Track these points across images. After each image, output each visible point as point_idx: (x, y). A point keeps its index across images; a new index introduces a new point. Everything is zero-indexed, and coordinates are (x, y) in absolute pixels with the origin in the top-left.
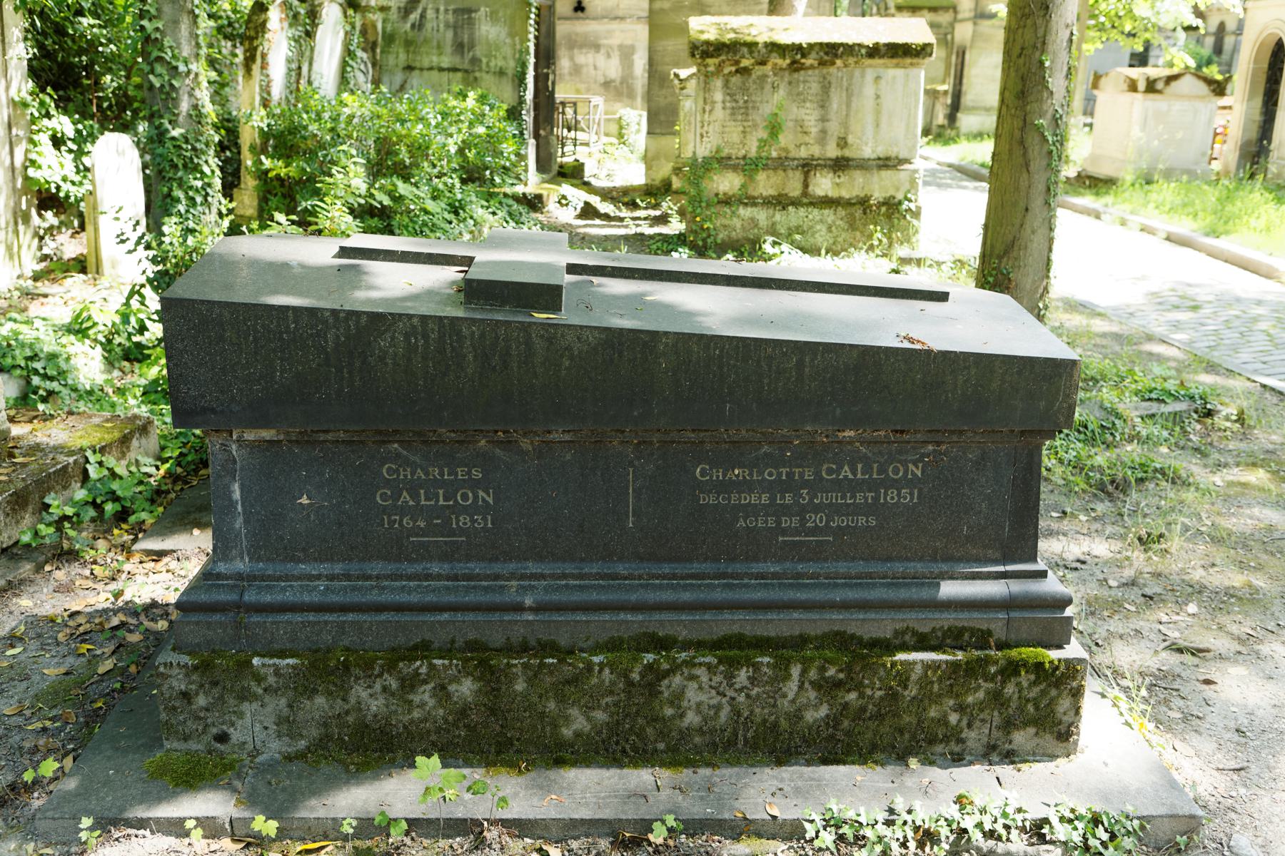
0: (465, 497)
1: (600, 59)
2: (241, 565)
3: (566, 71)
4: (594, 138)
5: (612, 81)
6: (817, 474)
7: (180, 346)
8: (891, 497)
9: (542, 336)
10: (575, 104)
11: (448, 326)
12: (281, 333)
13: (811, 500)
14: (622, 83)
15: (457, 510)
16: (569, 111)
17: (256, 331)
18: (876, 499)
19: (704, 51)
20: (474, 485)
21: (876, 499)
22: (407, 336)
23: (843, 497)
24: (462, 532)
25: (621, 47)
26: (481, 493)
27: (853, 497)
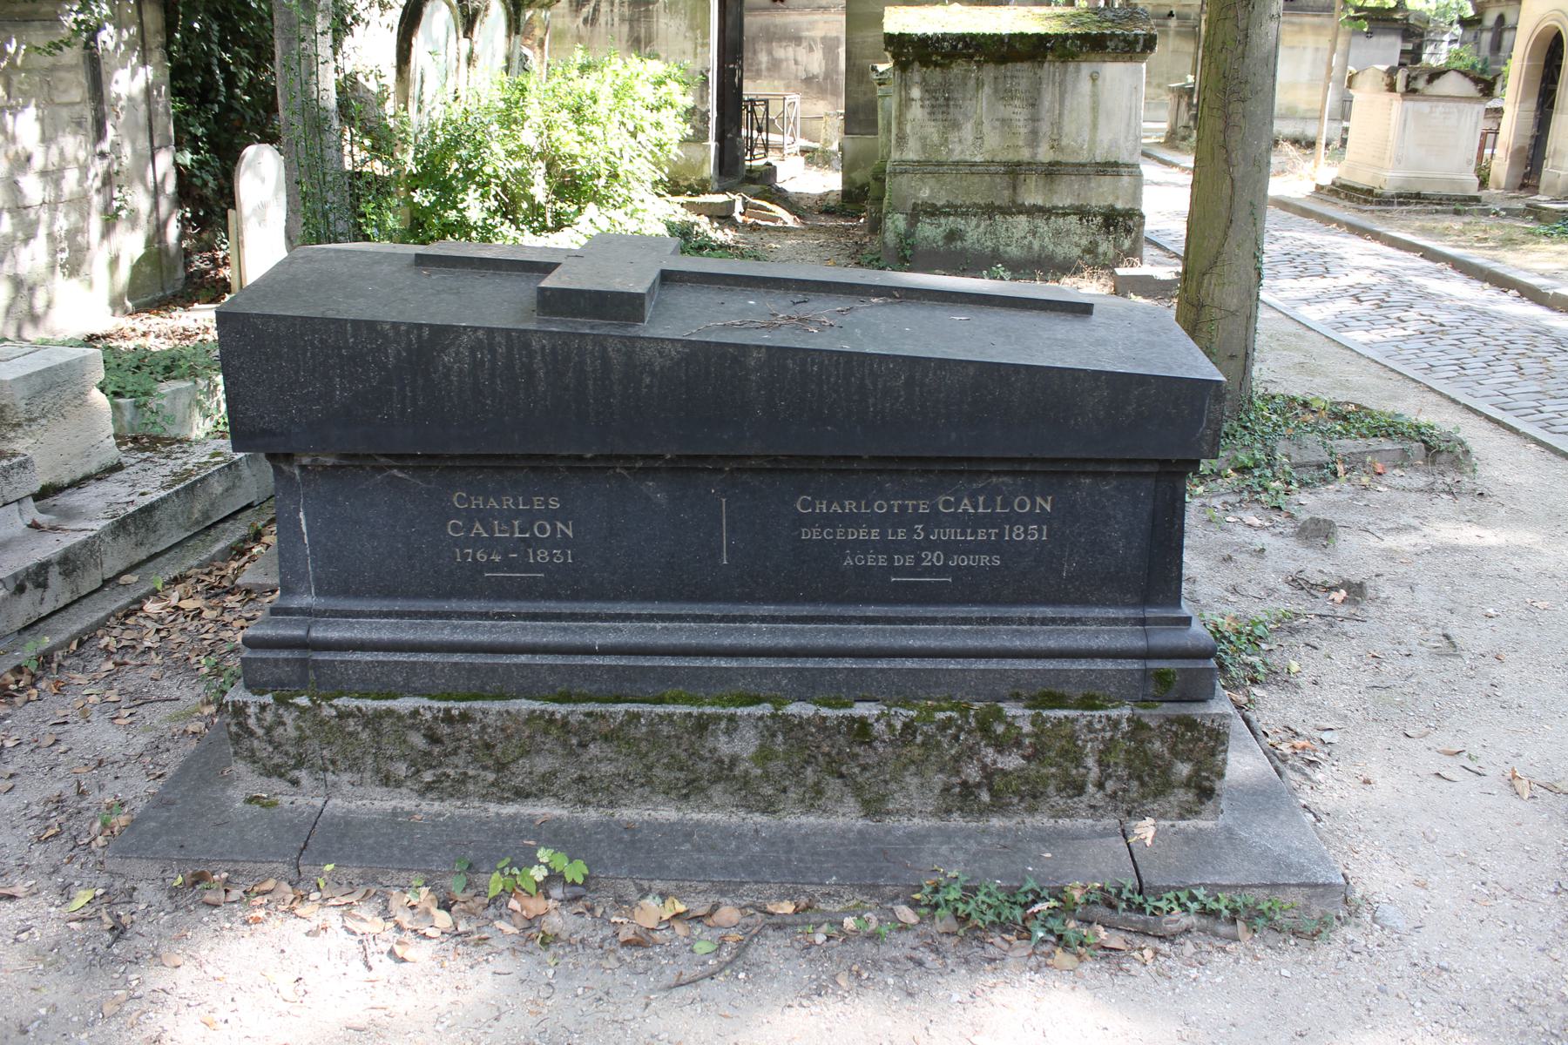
0: (542, 530)
1: (802, 53)
2: (308, 600)
3: (764, 66)
4: (788, 139)
5: (814, 77)
6: (934, 507)
7: (236, 363)
8: (1018, 533)
9: (619, 351)
10: (766, 102)
11: (516, 339)
12: (340, 348)
13: (927, 537)
14: (825, 79)
15: (533, 543)
16: (760, 110)
17: (312, 344)
18: (1000, 535)
19: (897, 43)
20: (552, 517)
21: (1000, 535)
22: (473, 351)
23: (964, 533)
24: (538, 567)
25: (824, 39)
26: (559, 525)
27: (974, 533)
